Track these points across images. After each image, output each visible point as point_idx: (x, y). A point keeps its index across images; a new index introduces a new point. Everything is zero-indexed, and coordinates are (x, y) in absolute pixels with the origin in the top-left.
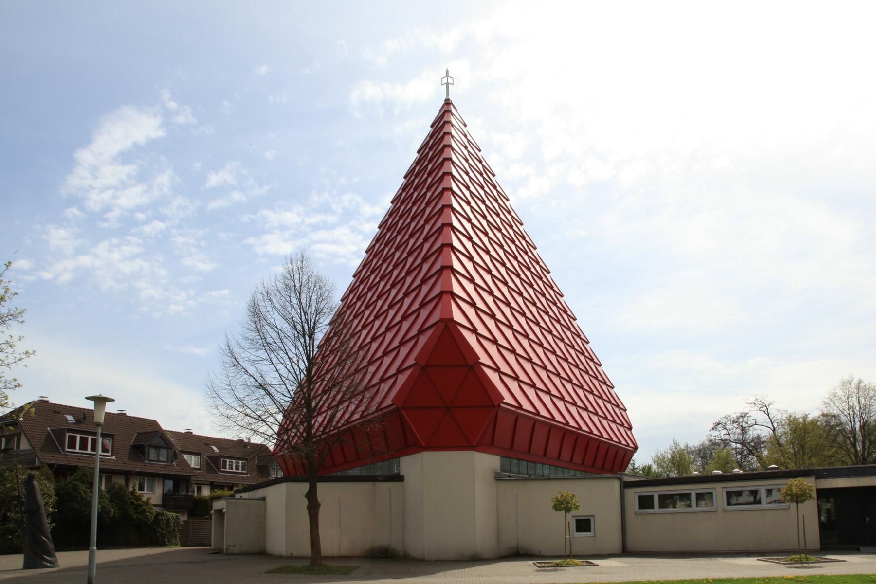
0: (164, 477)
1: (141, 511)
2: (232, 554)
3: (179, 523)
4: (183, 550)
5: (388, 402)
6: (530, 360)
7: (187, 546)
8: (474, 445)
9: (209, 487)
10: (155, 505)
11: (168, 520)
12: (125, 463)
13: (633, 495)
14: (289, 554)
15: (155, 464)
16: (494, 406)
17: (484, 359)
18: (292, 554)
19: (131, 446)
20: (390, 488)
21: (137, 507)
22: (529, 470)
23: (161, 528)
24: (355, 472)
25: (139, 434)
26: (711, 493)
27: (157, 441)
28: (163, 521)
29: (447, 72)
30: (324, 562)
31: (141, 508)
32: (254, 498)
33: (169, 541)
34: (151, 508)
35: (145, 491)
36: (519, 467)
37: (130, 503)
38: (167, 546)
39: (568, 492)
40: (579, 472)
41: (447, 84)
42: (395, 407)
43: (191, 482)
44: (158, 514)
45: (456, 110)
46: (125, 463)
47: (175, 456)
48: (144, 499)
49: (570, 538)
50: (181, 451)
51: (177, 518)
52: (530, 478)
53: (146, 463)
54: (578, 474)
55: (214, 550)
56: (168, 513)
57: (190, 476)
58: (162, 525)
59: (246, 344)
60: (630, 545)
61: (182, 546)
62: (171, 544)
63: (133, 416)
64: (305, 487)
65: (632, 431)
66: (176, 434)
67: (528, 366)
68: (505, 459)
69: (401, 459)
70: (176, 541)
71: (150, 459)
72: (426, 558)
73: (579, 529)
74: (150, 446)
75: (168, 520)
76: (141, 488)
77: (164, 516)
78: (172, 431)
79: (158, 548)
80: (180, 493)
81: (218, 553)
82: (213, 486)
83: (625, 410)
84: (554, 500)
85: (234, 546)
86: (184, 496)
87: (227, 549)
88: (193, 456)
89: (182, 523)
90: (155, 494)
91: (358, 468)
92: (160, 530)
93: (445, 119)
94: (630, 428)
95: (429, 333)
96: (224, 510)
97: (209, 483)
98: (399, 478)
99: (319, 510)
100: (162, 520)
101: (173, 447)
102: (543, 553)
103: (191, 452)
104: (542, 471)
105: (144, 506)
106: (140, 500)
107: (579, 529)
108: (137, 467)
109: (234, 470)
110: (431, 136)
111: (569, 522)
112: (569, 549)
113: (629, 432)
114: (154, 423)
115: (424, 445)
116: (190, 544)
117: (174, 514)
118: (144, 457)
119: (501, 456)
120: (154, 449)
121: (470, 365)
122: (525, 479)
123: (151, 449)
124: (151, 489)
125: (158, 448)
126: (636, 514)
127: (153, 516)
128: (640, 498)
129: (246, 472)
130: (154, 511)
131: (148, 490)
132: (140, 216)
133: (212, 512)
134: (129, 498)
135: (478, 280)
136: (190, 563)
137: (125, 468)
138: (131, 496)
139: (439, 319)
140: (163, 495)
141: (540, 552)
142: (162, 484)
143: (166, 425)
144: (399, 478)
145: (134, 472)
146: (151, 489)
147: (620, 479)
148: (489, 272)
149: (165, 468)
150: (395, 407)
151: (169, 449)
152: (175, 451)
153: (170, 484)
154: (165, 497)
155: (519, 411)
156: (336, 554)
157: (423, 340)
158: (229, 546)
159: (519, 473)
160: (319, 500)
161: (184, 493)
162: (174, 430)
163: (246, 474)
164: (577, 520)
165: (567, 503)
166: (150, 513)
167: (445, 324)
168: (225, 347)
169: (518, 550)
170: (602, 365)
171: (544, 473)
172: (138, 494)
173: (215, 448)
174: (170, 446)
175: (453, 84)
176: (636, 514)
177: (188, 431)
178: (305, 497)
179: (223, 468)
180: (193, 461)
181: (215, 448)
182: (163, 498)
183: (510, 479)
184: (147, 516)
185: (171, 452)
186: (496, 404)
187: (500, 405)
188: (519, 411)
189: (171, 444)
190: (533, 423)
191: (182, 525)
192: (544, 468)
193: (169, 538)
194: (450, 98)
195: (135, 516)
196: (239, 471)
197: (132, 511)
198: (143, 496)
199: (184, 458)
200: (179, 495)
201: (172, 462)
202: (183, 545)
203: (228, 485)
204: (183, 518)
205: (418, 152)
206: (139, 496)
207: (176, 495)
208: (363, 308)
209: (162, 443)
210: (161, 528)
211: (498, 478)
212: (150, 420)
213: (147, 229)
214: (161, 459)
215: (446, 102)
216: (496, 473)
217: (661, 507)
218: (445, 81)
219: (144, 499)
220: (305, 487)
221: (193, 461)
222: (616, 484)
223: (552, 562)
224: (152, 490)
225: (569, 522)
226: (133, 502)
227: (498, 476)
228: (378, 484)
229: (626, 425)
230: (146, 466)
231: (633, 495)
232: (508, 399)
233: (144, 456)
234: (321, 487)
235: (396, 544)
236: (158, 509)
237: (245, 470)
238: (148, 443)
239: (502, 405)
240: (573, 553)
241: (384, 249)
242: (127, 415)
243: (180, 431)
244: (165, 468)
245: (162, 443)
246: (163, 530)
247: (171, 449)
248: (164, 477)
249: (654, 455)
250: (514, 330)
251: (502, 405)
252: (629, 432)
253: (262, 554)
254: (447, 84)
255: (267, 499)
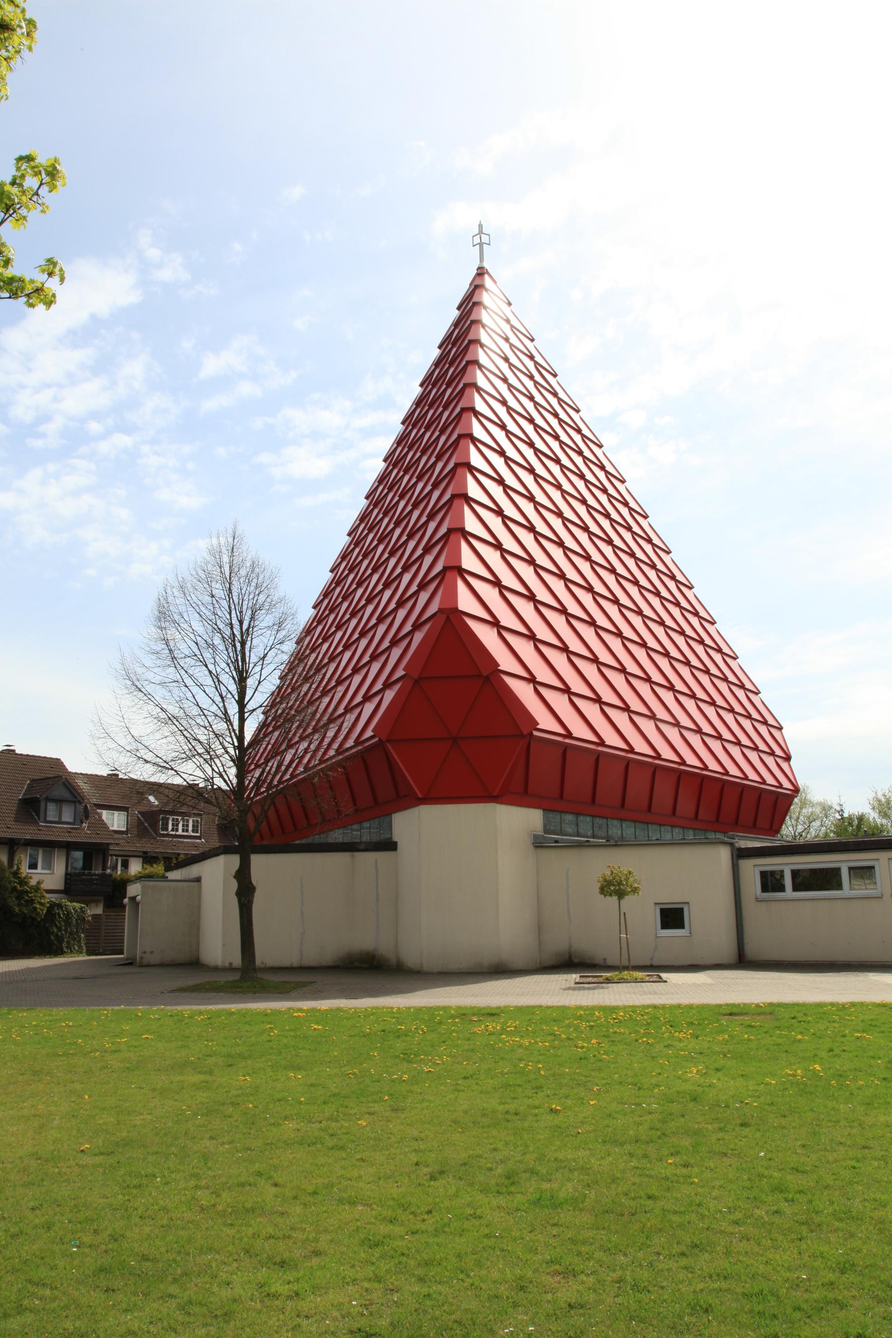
0: (69, 847)
1: (27, 901)
2: (149, 966)
3: (84, 918)
4: (89, 960)
5: (369, 733)
6: (682, 633)
7: (96, 955)
8: (495, 794)
9: (141, 860)
10: (49, 891)
11: (68, 912)
12: (8, 828)
13: (752, 869)
14: (227, 965)
15: (54, 827)
16: (522, 736)
17: (506, 662)
18: (231, 964)
19: (20, 800)
20: (376, 861)
21: (20, 895)
22: (596, 829)
23: (56, 926)
24: (337, 836)
25: (33, 781)
26: (873, 867)
27: (60, 792)
28: (60, 917)
29: (480, 226)
30: (260, 975)
31: (27, 896)
32: (187, 878)
33: (69, 947)
34: (43, 896)
35: (39, 870)
36: (577, 825)
37: (10, 890)
38: (65, 955)
39: (619, 867)
40: (691, 832)
41: (481, 244)
42: (377, 739)
43: (111, 852)
44: (53, 905)
45: (495, 282)
46: (8, 828)
47: (87, 814)
48: (33, 882)
49: (627, 938)
50: (95, 805)
51: (82, 911)
52: (608, 843)
53: (41, 826)
54: (690, 835)
55: (127, 959)
56: (69, 904)
57: (108, 844)
58: (58, 922)
59: (149, 661)
60: (753, 949)
61: (88, 955)
62: (71, 951)
63: (25, 753)
64: (234, 861)
65: (792, 762)
66: (93, 779)
67: (680, 640)
68: (551, 815)
69: (393, 815)
70: (80, 947)
71: (48, 819)
72: (425, 969)
73: (665, 925)
74: (48, 800)
75: (68, 915)
76: (33, 866)
77: (62, 907)
78: (86, 774)
79: (51, 958)
80: (93, 872)
81: (131, 964)
82: (148, 859)
83: (780, 729)
84: (601, 879)
85: (152, 952)
86: (98, 875)
87: (142, 958)
88: (116, 813)
89: (90, 918)
90: (53, 873)
91: (341, 831)
92: (55, 930)
93: (475, 299)
94: (788, 758)
95: (426, 628)
96: (139, 898)
97: (141, 854)
98: (390, 846)
99: (253, 897)
100: (59, 914)
101: (83, 799)
102: (609, 963)
103: (113, 806)
104: (619, 832)
105: (31, 893)
106: (26, 883)
107: (665, 925)
108: (27, 832)
109: (180, 832)
110: (456, 324)
111: (624, 914)
112: (627, 957)
113: (784, 765)
114: (57, 763)
115: (420, 796)
116: (101, 950)
117: (77, 905)
118: (38, 815)
119: (544, 810)
120: (54, 804)
121: (485, 675)
122: (579, 845)
123: (49, 804)
124: (48, 865)
125: (59, 801)
126: (758, 900)
127: (45, 909)
128: (763, 874)
129: (198, 834)
130: (47, 900)
131: (43, 868)
132: (95, 427)
133: (126, 900)
134: (10, 882)
135: (591, 501)
136: (77, 978)
137: (8, 836)
138: (12, 879)
139: (437, 610)
140: (67, 874)
141: (605, 960)
142: (65, 858)
143: (74, 765)
144: (390, 846)
145: (23, 841)
146: (48, 865)
147: (732, 844)
148: (605, 491)
149: (69, 832)
150: (377, 739)
151: (77, 804)
152: (86, 806)
153: (78, 855)
154: (69, 878)
155: (567, 741)
156: (295, 962)
157: (418, 637)
158: (145, 952)
159: (578, 836)
160: (254, 882)
161: (100, 872)
162: (89, 773)
163: (199, 838)
164: (662, 910)
165: (620, 883)
166: (41, 904)
167: (446, 616)
168: (119, 667)
169: (570, 957)
170: (738, 658)
171: (624, 835)
172: (24, 875)
173: (152, 799)
174: (80, 799)
175: (489, 244)
176: (758, 900)
177: (112, 772)
178: (235, 877)
179: (162, 830)
180: (116, 821)
181: (152, 799)
182: (66, 879)
183: (557, 845)
184: (35, 909)
185: (81, 808)
186: (525, 732)
187: (531, 733)
188: (567, 741)
189: (79, 795)
190: (595, 757)
191: (89, 921)
192: (624, 825)
193: (68, 942)
194: (486, 265)
195: (17, 909)
196: (177, 833)
197: (12, 902)
198: (31, 878)
199: (101, 817)
200: (90, 874)
201: (82, 823)
202: (89, 953)
203: (164, 856)
204: (99, 910)
205: (440, 347)
206: (25, 878)
207: (86, 875)
208: (419, 552)
209: (66, 795)
210: (56, 926)
211: (539, 843)
212: (51, 758)
213: (103, 447)
214: (64, 819)
215: (479, 272)
216: (535, 836)
217: (796, 888)
218: (477, 240)
219: (33, 882)
220: (234, 861)
221: (116, 821)
222: (724, 854)
223: (601, 976)
224: (50, 869)
225: (624, 914)
226: (15, 887)
227: (538, 841)
228: (356, 854)
229: (778, 752)
230: (40, 830)
231: (752, 869)
232: (545, 722)
233: (38, 815)
234: (258, 861)
235: (384, 947)
236: (53, 898)
237: (197, 832)
238: (45, 796)
239: (536, 733)
240: (634, 962)
241: (435, 464)
242: (17, 752)
243: (99, 773)
244: (69, 832)
245: (66, 795)
246: (60, 929)
247: (80, 803)
248: (69, 847)
249: (871, 795)
250: (640, 587)
251: (536, 733)
252: (784, 765)
253: (194, 964)
254: (481, 244)
255: (203, 880)
